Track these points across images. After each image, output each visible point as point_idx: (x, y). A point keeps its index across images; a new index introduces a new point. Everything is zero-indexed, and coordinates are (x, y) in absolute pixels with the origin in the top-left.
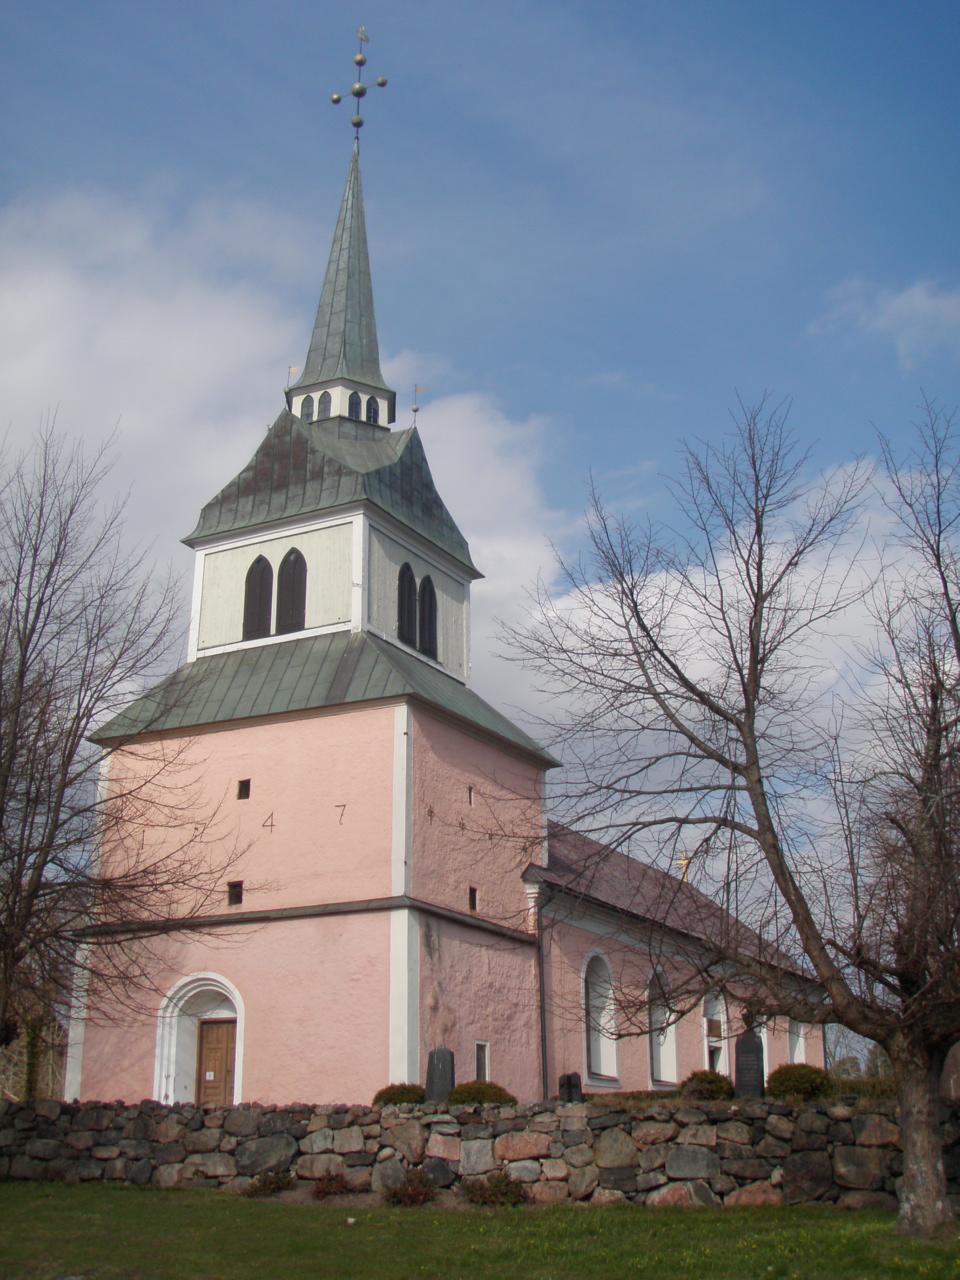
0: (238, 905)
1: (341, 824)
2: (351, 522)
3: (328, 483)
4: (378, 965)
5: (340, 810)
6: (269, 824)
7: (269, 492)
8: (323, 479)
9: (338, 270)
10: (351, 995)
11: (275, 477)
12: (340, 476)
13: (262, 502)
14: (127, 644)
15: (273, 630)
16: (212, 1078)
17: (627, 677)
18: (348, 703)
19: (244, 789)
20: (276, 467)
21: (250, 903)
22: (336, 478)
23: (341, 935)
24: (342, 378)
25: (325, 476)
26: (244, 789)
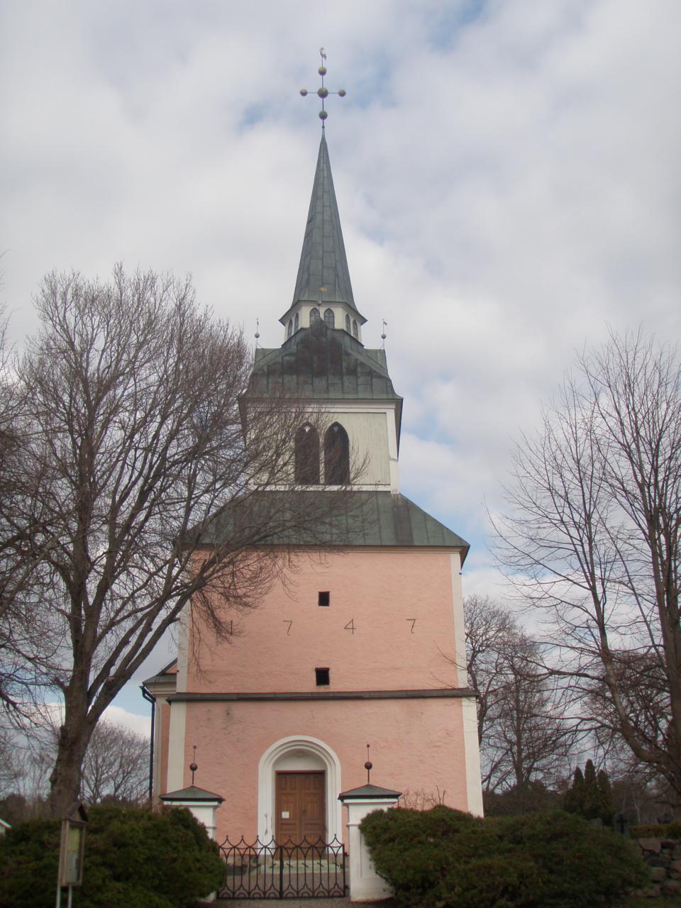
0: (326, 686)
1: (413, 633)
2: (385, 413)
3: (361, 380)
4: (455, 734)
5: (411, 623)
6: (350, 627)
7: (311, 376)
8: (357, 377)
9: (323, 221)
10: (434, 757)
11: (315, 365)
12: (372, 378)
13: (305, 383)
14: (674, 450)
15: (322, 481)
16: (671, 717)
17: (626, 546)
18: (356, 546)
19: (324, 599)
20: (315, 358)
21: (335, 685)
22: (369, 378)
23: (422, 713)
24: (346, 303)
25: (359, 375)
26: (324, 599)
